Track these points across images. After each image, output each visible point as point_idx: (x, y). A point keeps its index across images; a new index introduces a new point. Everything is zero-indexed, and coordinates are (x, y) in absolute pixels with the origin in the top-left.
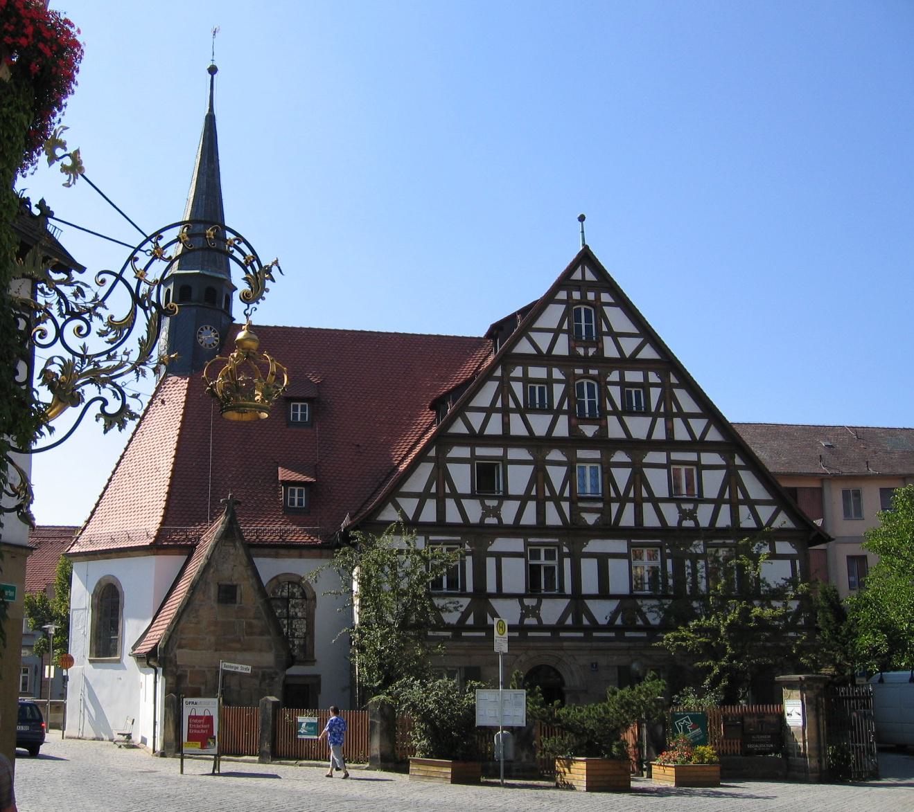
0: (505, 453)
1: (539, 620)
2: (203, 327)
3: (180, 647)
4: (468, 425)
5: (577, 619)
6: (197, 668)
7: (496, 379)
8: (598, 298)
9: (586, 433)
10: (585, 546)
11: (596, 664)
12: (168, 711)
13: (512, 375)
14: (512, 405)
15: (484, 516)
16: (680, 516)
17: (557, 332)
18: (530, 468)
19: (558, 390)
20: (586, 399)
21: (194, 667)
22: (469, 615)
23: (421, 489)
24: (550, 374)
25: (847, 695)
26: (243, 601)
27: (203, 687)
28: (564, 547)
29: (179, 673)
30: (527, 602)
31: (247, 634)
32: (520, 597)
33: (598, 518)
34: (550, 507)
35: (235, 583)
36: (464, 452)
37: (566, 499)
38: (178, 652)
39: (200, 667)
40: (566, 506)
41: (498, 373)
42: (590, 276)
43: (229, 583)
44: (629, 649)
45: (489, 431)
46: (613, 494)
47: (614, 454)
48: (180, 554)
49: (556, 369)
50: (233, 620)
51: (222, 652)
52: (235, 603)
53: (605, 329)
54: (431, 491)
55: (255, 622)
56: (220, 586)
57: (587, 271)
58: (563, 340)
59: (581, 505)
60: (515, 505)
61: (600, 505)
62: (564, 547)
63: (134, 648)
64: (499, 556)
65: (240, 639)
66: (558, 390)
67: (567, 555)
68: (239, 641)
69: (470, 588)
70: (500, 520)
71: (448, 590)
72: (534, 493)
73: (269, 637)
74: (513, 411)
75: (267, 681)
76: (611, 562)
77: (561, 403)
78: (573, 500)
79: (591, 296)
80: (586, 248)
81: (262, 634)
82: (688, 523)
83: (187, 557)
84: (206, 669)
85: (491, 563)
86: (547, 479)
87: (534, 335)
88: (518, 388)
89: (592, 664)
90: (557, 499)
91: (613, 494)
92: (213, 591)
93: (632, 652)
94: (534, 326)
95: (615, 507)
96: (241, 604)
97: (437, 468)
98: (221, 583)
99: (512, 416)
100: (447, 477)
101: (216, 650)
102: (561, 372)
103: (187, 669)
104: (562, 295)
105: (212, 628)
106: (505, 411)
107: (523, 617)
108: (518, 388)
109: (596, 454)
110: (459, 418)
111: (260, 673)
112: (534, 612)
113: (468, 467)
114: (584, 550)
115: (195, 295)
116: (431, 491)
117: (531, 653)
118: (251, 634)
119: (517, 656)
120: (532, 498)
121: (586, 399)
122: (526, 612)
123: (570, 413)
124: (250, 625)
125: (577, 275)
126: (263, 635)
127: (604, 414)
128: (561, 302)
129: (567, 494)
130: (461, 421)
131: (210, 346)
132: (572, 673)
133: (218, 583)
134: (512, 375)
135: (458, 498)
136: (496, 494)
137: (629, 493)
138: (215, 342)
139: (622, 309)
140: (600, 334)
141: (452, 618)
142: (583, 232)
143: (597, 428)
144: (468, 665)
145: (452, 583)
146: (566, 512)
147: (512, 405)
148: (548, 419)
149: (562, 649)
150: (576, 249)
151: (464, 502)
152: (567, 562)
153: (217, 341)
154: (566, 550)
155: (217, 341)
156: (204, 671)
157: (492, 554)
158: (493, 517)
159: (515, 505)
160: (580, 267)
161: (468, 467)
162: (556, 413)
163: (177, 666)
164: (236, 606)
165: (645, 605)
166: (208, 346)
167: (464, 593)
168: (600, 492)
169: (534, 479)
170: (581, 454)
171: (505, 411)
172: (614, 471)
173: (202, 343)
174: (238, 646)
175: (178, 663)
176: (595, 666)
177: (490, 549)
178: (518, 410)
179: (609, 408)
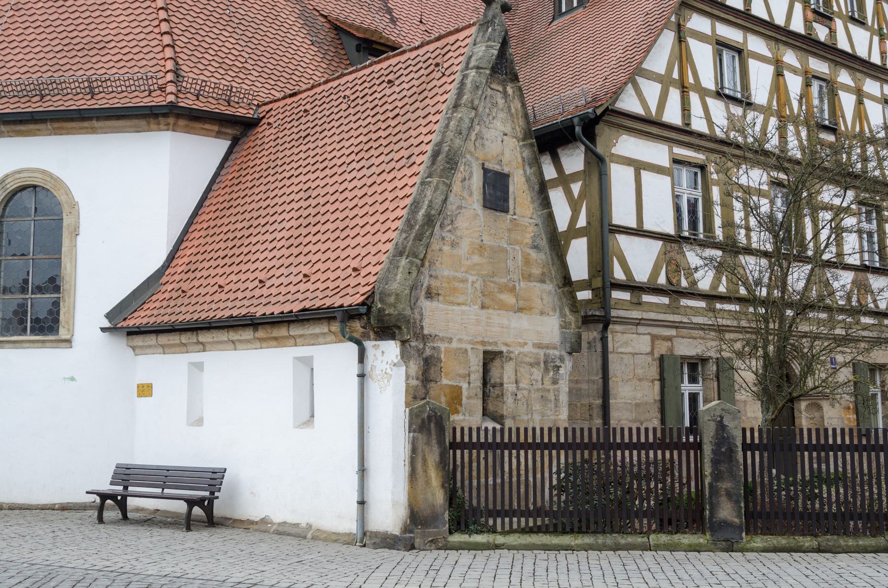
12: (420, 445)
25: (834, 508)
29: (428, 352)
35: (506, 170)
38: (426, 305)
48: (219, 135)
51: (490, 311)
63: (359, 274)
83: (229, 142)
84: (469, 347)
96: (515, 214)
101: (483, 307)
105: (476, 259)
111: (542, 357)
133: (483, 164)
137: (659, 275)
163: (425, 338)
164: (509, 217)
165: (852, 206)
175: (426, 332)
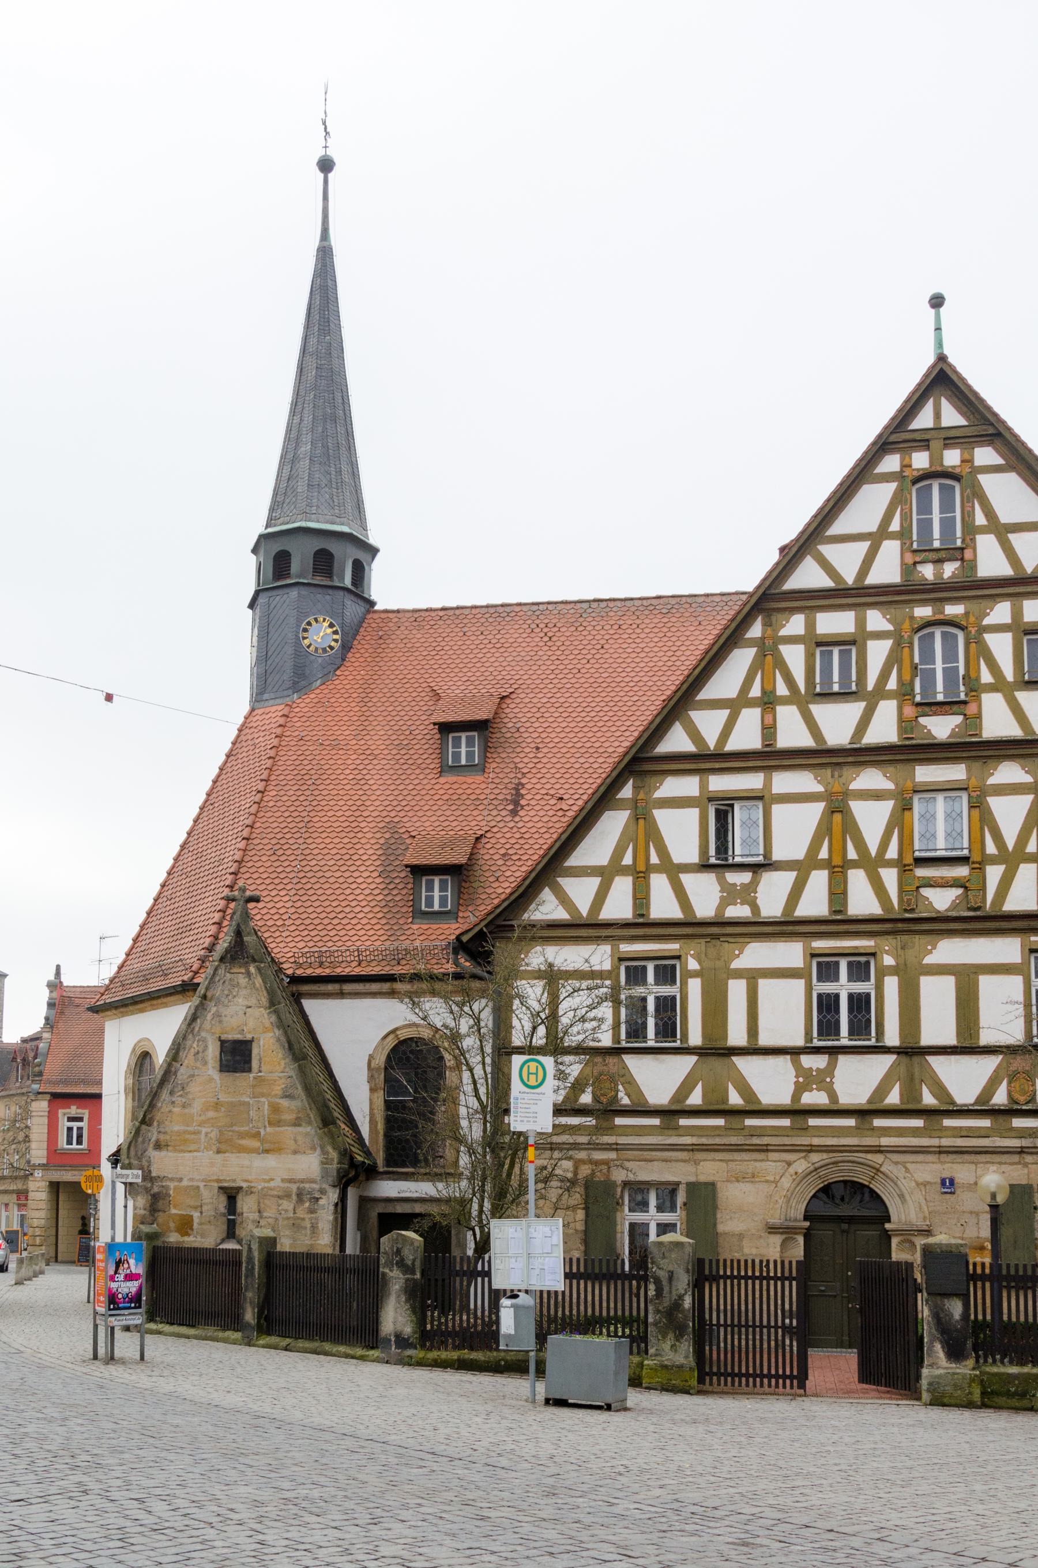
0: (768, 783)
1: (833, 1096)
2: (311, 619)
3: (158, 1146)
4: (695, 735)
5: (911, 1091)
6: (185, 1183)
7: (752, 642)
8: (967, 461)
9: (934, 732)
10: (930, 952)
11: (952, 1181)
13: (783, 632)
14: (782, 690)
15: (724, 903)
16: (721, 898)
17: (876, 539)
18: (817, 809)
19: (878, 652)
20: (939, 666)
21: (181, 1180)
22: (694, 1087)
23: (604, 862)
24: (861, 623)
26: (263, 1068)
27: (196, 1215)
28: (885, 956)
29: (156, 1190)
30: (808, 1061)
31: (270, 1124)
32: (793, 1052)
33: (957, 897)
34: (858, 881)
35: (249, 1037)
36: (687, 786)
37: (889, 864)
39: (191, 1180)
40: (890, 877)
41: (756, 630)
42: (952, 417)
43: (239, 1037)
44: (1022, 1151)
45: (735, 743)
46: (991, 848)
47: (995, 769)
49: (876, 612)
50: (247, 1100)
51: (227, 1155)
52: (250, 1070)
53: (980, 519)
54: (624, 863)
55: (285, 1103)
56: (223, 1042)
57: (945, 404)
58: (890, 552)
59: (921, 872)
60: (788, 878)
61: (962, 871)
62: (885, 956)
64: (753, 977)
65: (259, 1133)
66: (878, 652)
67: (894, 971)
68: (257, 1135)
69: (695, 1038)
70: (755, 908)
71: (657, 1042)
72: (824, 854)
73: (309, 1129)
74: (785, 701)
75: (307, 1204)
76: (985, 982)
77: (884, 676)
78: (905, 866)
79: (952, 458)
80: (942, 358)
81: (297, 1123)
82: (738, 911)
85: (737, 991)
86: (851, 828)
87: (826, 550)
88: (794, 657)
89: (943, 1182)
90: (872, 865)
91: (991, 848)
92: (213, 1051)
93: (1029, 1159)
94: (828, 533)
95: (994, 874)
97: (636, 818)
98: (224, 1037)
99: (782, 711)
100: (654, 835)
101: (218, 1152)
102: (884, 617)
103: (168, 1183)
104: (891, 463)
105: (211, 1114)
106: (768, 702)
107: (799, 1090)
108: (794, 657)
109: (956, 772)
110: (677, 723)
112: (823, 1080)
113: (694, 813)
114: (928, 960)
115: (295, 566)
116: (624, 863)
117: (815, 1157)
118: (278, 1123)
119: (789, 1164)
120: (624, 871)
121: (939, 666)
122: (806, 1081)
123: (904, 693)
124: (275, 1109)
125: (924, 420)
126: (300, 1125)
127: (975, 688)
128: (886, 478)
129: (892, 853)
130: (681, 728)
131: (324, 650)
132: (902, 1196)
134: (783, 632)
135: (674, 871)
136: (730, 861)
138: (333, 644)
139: (1019, 474)
140: (971, 531)
141: (660, 1093)
142: (938, 329)
143: (958, 719)
144: (692, 1179)
145: (667, 1029)
146: (887, 885)
147: (782, 690)
148: (855, 709)
149: (878, 1150)
150: (922, 363)
151: (686, 879)
152: (891, 984)
153: (336, 641)
154: (888, 961)
155: (336, 641)
156: (198, 1187)
157: (739, 974)
158: (742, 904)
159: (788, 878)
160: (931, 401)
161: (694, 813)
162: (873, 699)
164: (251, 1075)
166: (320, 651)
167: (685, 1045)
168: (966, 845)
169: (824, 830)
170: (926, 773)
171: (768, 702)
172: (995, 803)
173: (309, 647)
174: (255, 1144)
175: (154, 1174)
176: (948, 1185)
177: (735, 964)
178: (795, 697)
179: (986, 677)
